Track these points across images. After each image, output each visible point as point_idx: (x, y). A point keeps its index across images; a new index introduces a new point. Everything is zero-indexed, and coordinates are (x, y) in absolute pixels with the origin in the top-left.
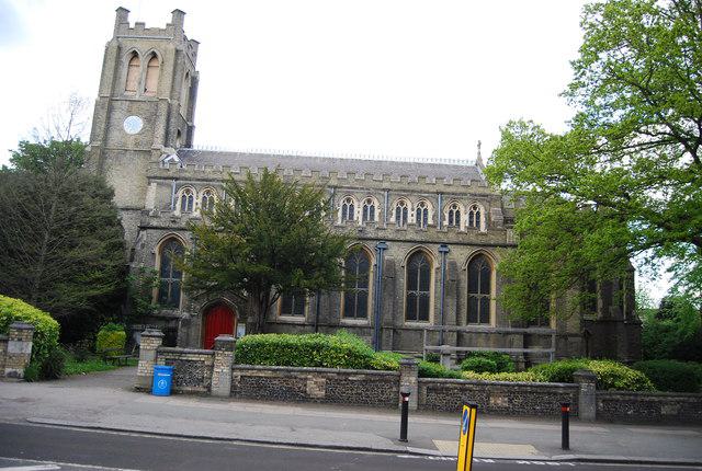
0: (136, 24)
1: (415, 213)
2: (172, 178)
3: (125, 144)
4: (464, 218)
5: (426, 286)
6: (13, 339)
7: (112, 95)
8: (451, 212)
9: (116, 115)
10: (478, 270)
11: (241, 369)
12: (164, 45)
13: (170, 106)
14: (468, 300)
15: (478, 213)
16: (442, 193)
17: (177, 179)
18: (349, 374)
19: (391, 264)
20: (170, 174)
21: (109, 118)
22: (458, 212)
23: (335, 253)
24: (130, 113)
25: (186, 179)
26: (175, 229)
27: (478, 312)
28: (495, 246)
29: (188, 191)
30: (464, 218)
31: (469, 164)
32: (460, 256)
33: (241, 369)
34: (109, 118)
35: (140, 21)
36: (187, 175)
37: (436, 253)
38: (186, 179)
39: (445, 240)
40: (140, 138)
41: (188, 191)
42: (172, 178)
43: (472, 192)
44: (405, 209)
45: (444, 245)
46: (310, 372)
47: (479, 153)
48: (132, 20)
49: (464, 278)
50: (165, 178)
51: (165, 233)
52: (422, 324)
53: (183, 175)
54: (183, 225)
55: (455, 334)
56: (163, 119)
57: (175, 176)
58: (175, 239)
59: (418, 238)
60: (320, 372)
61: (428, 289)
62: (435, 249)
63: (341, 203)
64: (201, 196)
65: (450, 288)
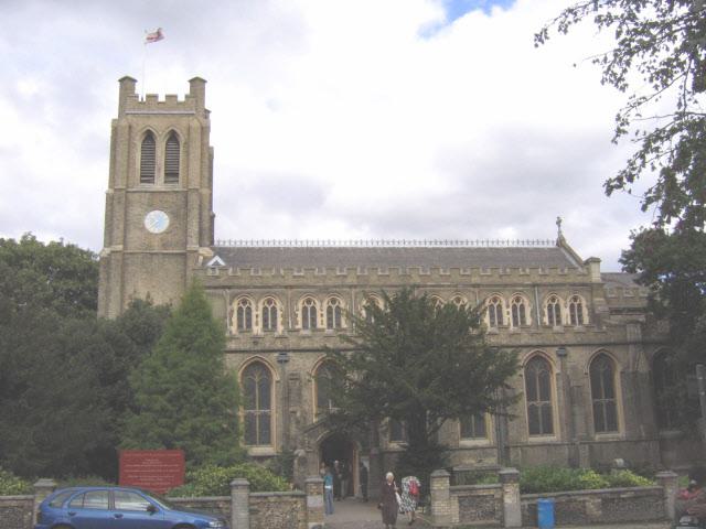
0: (167, 97)
1: (510, 310)
2: (224, 287)
3: (150, 246)
4: (565, 312)
5: (546, 395)
6: (312, 494)
7: (127, 186)
8: (550, 306)
9: (135, 211)
10: (601, 367)
11: (528, 499)
12: (184, 122)
13: (201, 195)
14: (594, 406)
15: (579, 305)
16: (538, 285)
17: (229, 288)
18: (620, 493)
19: (295, 377)
20: (221, 282)
21: (126, 214)
22: (522, 305)
23: (510, 368)
24: (152, 207)
25: (241, 287)
26: (258, 352)
27: (605, 420)
28: (615, 344)
29: (244, 302)
30: (565, 312)
31: (551, 246)
32: (580, 358)
33: (528, 499)
34: (126, 214)
35: (151, 92)
36: (243, 282)
37: (554, 357)
38: (241, 287)
39: (563, 342)
40: (169, 237)
41: (244, 302)
42: (224, 287)
43: (570, 281)
44: (499, 306)
45: (562, 346)
46: (587, 494)
47: (560, 232)
48: (142, 90)
49: (587, 382)
50: (216, 288)
51: (248, 357)
52: (610, 436)
53: (236, 282)
54: (267, 345)
55: (587, 446)
56: (195, 212)
57: (226, 284)
58: (603, 354)
59: (534, 341)
60: (596, 494)
61: (268, 407)
62: (552, 353)
63: (300, 306)
64: (261, 307)
65: (572, 396)
